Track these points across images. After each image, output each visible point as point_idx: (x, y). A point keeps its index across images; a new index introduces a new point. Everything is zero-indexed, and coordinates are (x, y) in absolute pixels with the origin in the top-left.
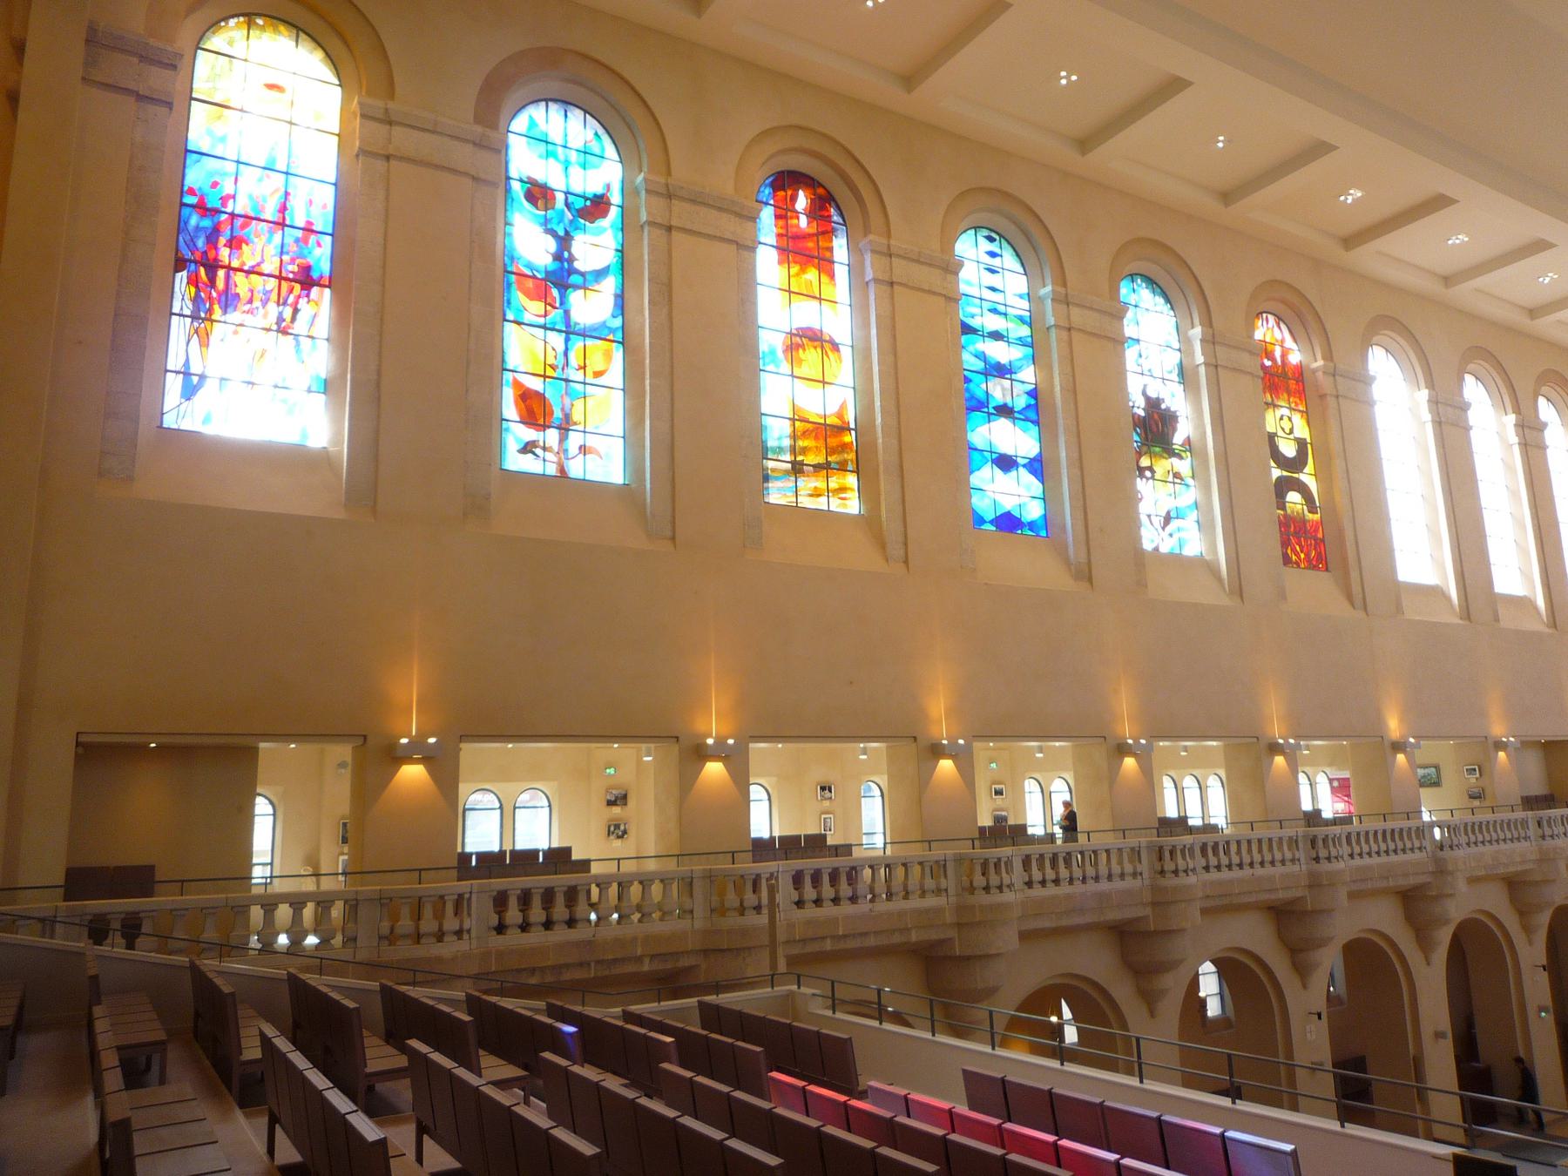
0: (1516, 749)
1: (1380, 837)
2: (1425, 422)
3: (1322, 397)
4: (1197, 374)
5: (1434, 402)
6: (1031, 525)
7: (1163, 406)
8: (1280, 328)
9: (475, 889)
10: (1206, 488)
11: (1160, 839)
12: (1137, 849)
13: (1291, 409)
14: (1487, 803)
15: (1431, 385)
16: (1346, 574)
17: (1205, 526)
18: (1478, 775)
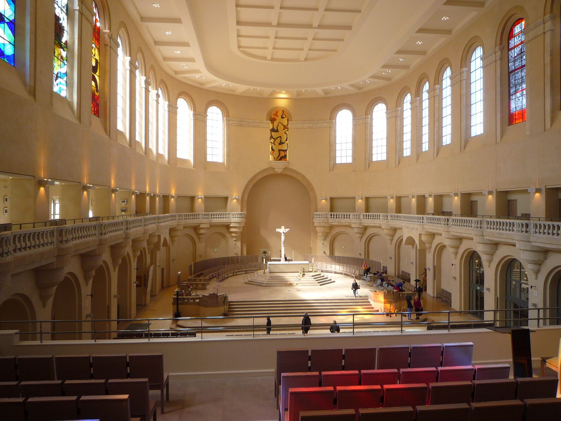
0: (176, 198)
1: (187, 216)
2: (127, 69)
3: (106, 45)
4: (74, 14)
5: (169, 106)
6: (8, 56)
7: (60, 22)
8: (95, 8)
9: (55, 229)
10: (71, 67)
11: (90, 223)
12: (53, 231)
13: (96, 46)
14: (127, 213)
15: (169, 101)
16: (106, 120)
17: (69, 85)
18: (126, 203)
